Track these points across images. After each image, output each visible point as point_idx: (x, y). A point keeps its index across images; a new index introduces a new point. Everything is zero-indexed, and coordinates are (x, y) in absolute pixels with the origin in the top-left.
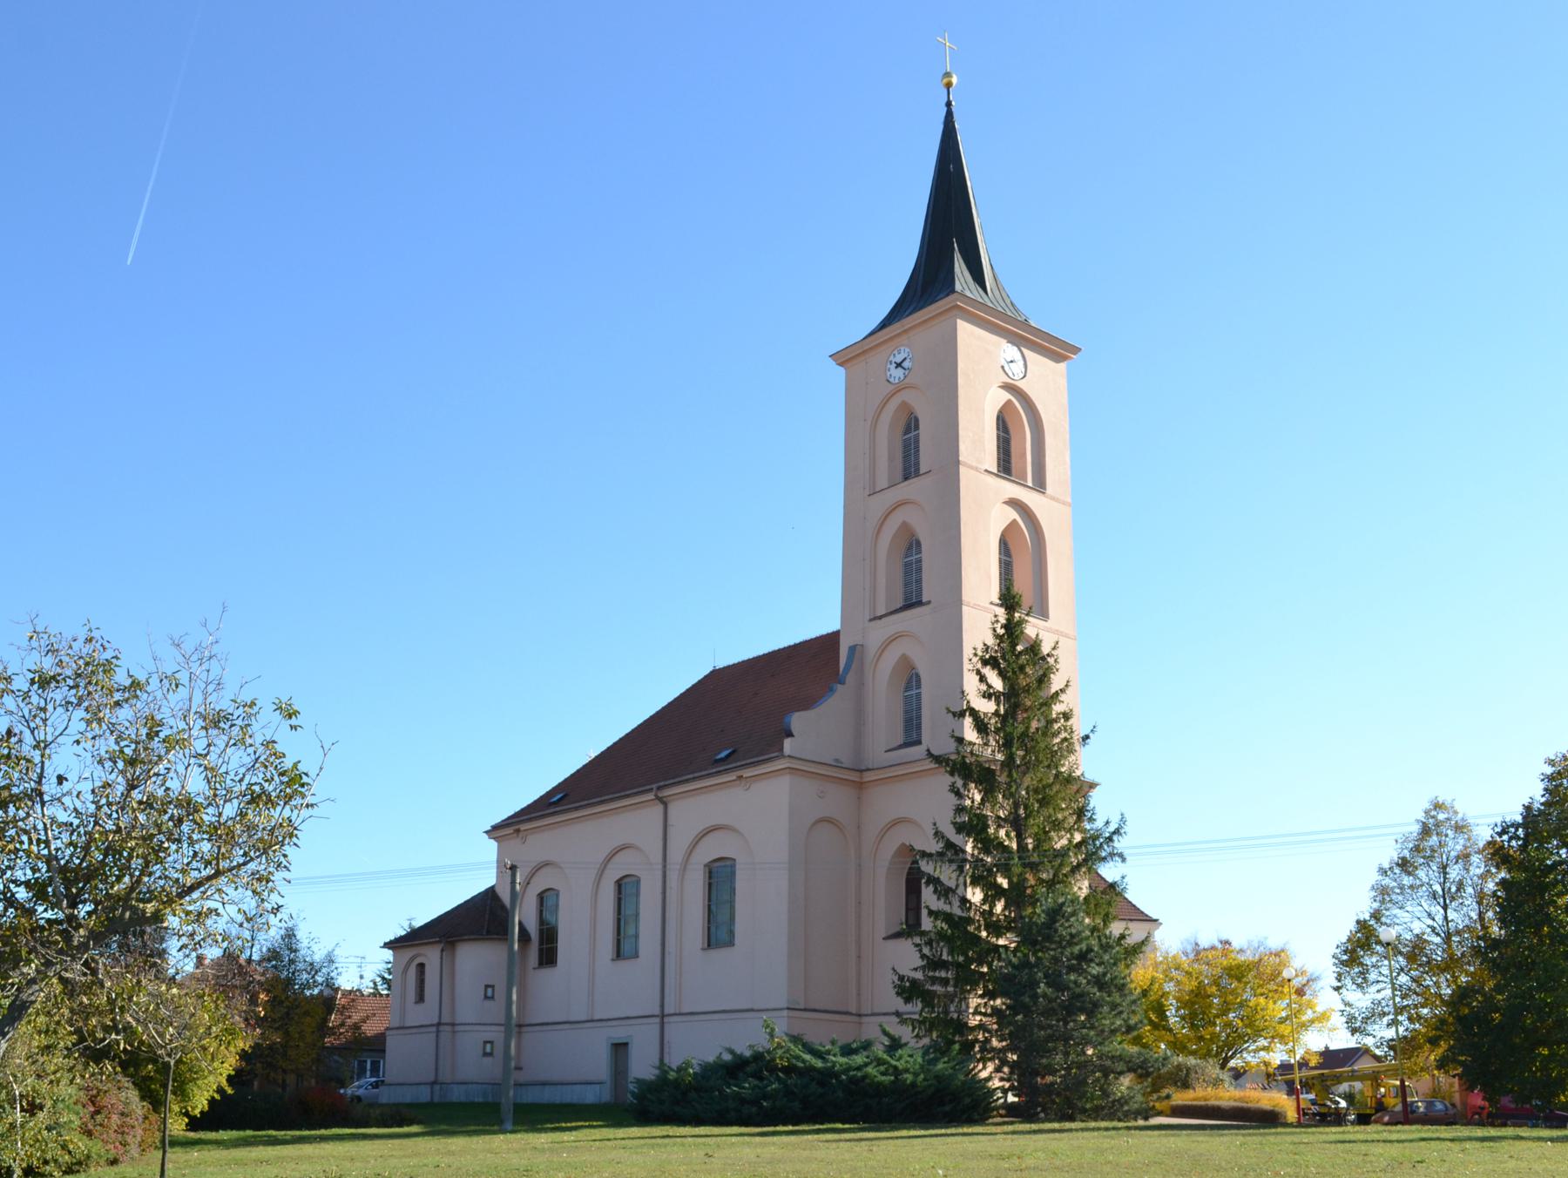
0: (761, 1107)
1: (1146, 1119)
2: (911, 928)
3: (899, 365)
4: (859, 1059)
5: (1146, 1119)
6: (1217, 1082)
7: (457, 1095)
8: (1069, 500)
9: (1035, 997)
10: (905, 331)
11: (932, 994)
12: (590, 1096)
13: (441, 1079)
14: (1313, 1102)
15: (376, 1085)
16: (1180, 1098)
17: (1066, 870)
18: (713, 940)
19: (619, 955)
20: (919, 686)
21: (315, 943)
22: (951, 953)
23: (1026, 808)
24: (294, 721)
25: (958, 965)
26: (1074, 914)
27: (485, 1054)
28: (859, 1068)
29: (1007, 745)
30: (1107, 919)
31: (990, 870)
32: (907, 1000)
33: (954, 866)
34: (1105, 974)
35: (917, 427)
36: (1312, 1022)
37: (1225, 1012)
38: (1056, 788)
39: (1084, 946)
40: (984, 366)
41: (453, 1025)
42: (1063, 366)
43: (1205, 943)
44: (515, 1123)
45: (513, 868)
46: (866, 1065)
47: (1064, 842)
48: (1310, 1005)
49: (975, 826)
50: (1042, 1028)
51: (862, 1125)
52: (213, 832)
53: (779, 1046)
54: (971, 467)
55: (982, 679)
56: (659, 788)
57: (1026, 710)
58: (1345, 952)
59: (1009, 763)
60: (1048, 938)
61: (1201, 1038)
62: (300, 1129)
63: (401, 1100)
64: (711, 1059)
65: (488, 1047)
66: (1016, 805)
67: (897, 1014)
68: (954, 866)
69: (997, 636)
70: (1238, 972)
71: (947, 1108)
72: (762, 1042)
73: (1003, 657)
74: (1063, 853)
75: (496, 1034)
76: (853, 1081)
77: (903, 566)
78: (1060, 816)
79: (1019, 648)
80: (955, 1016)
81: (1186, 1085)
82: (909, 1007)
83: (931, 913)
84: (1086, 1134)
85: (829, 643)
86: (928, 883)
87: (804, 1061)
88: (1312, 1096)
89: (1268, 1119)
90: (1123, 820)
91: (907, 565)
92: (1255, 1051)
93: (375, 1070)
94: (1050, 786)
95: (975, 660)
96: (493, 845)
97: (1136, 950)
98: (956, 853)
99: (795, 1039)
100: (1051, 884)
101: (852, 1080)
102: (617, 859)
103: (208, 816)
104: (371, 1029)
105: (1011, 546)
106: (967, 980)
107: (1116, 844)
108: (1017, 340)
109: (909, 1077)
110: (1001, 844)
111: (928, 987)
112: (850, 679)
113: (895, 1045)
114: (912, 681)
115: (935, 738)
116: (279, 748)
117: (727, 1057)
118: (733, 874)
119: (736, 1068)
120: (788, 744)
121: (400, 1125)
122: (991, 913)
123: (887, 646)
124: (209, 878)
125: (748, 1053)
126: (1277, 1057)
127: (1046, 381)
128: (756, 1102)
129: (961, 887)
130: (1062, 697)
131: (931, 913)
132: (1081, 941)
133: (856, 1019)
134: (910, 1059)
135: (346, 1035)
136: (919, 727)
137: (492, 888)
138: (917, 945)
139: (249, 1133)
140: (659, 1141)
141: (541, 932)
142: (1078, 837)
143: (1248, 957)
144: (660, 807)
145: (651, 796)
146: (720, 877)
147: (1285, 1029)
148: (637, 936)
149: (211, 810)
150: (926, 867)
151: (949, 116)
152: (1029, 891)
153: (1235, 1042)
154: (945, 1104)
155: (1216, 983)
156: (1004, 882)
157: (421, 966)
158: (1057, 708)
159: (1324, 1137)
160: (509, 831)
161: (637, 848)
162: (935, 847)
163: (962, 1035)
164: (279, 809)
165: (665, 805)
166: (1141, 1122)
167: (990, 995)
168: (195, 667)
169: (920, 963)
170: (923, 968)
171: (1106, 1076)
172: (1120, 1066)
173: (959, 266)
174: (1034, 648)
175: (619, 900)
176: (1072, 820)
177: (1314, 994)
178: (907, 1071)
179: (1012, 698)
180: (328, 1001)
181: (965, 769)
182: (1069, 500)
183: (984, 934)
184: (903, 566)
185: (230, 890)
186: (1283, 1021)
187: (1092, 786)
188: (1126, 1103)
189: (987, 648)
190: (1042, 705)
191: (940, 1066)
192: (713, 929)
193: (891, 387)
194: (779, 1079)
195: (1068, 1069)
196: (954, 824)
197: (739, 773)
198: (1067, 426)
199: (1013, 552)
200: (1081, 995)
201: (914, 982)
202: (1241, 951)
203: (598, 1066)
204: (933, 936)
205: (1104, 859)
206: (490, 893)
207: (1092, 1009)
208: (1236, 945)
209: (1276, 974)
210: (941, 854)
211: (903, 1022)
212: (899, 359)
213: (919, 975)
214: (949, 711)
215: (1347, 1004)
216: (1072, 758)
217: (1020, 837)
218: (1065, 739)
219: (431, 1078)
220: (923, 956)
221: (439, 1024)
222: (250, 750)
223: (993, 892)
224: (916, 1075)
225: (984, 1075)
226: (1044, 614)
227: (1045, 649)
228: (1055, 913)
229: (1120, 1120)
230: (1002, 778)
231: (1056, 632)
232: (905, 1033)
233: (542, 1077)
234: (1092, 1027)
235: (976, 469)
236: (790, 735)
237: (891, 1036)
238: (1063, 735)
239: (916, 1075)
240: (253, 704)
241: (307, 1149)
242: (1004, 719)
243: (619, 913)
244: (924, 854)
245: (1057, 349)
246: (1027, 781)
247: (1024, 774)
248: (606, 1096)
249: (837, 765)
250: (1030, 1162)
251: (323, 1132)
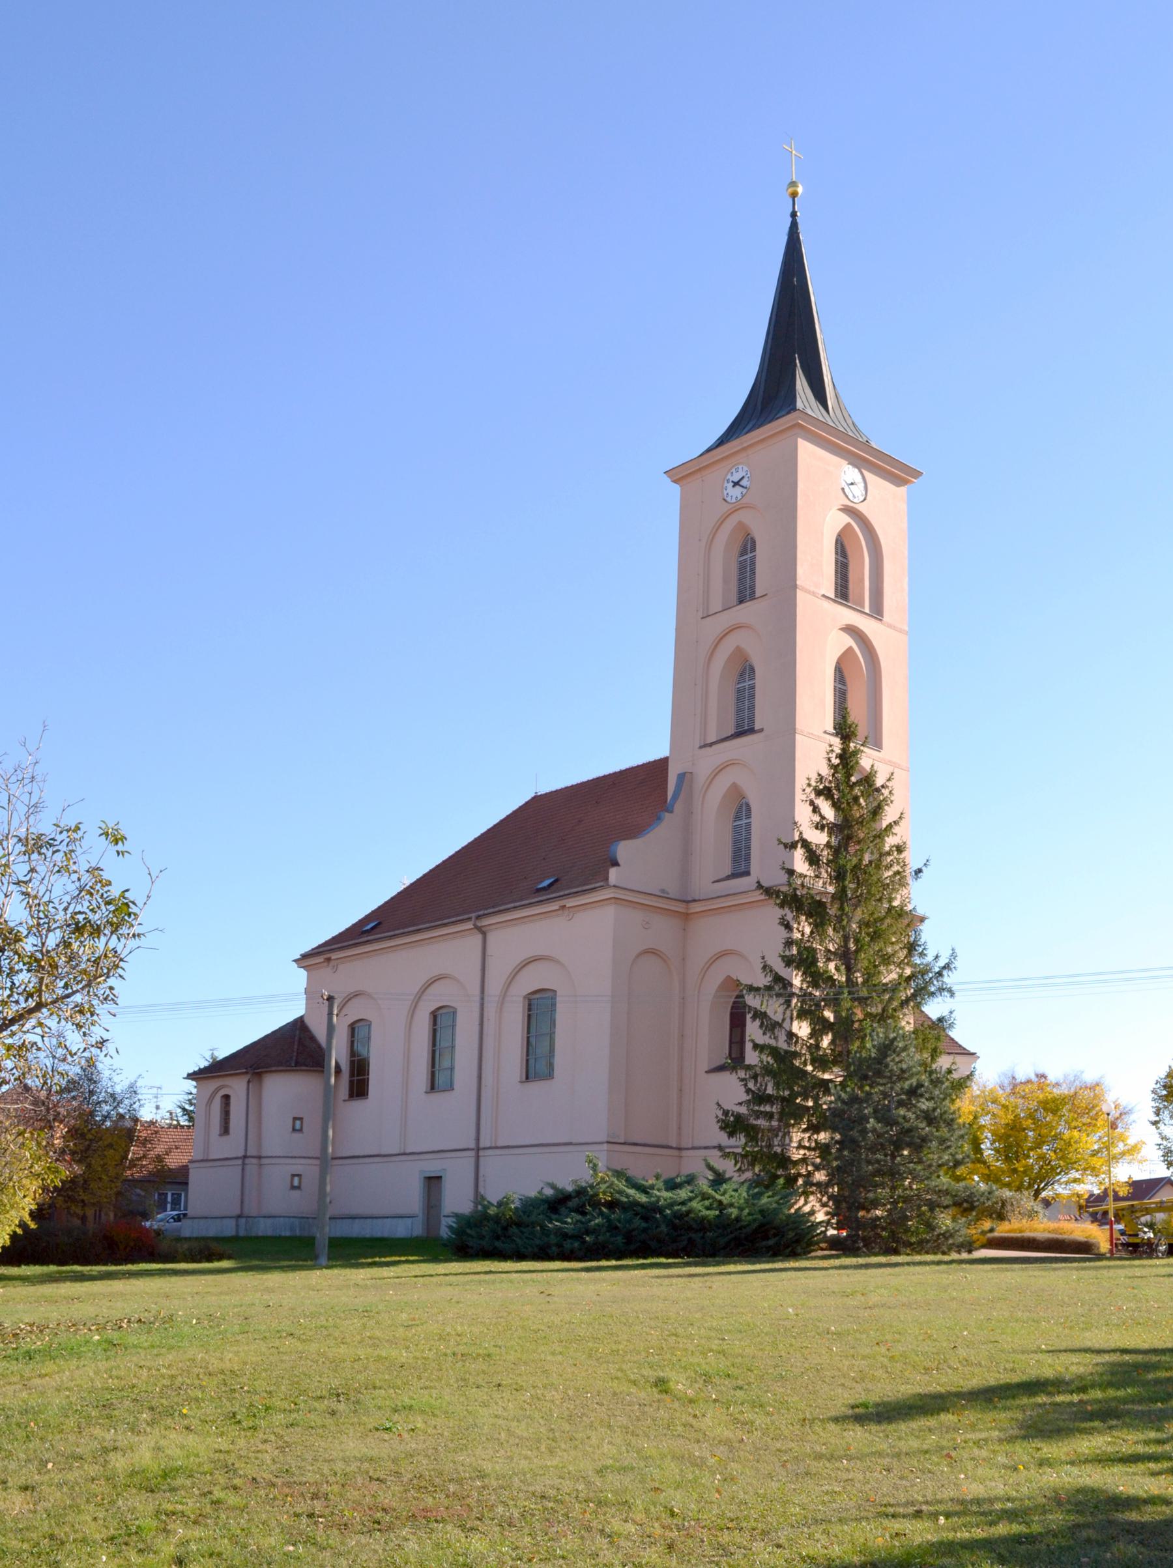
0: (584, 1242)
1: (970, 1252)
2: (735, 1061)
3: (736, 484)
4: (683, 1194)
5: (970, 1252)
6: (1031, 1214)
7: (264, 1228)
8: (906, 628)
9: (864, 1132)
10: (744, 449)
11: (756, 1129)
12: (401, 1230)
13: (246, 1212)
14: (1123, 1233)
15: (178, 1219)
16: (1003, 1230)
17: (895, 1004)
18: (532, 1072)
19: (433, 1087)
20: (749, 815)
21: (116, 1073)
22: (777, 1086)
23: (857, 941)
24: (120, 847)
25: (783, 1099)
26: (905, 1049)
27: (293, 1188)
28: (683, 1203)
29: (839, 876)
30: (935, 1053)
31: (818, 1005)
32: (731, 1134)
33: (782, 1000)
34: (934, 1109)
35: (753, 549)
36: (1123, 1154)
37: (1038, 1145)
38: (888, 921)
39: (914, 1081)
40: (826, 487)
41: (260, 1157)
42: (903, 490)
43: (1021, 1077)
44: (329, 1259)
45: (330, 999)
46: (691, 1199)
47: (894, 976)
48: (1122, 1138)
49: (805, 961)
50: (869, 1162)
51: (686, 1259)
52: (34, 963)
53: (603, 1181)
54: (809, 592)
55: (816, 809)
56: (478, 917)
57: (859, 842)
58: (1165, 1087)
59: (840, 896)
60: (879, 1073)
61: (1015, 1171)
62: (105, 1264)
63: (204, 1234)
64: (533, 1194)
65: (296, 1180)
66: (846, 939)
67: (720, 1148)
68: (782, 1000)
69: (832, 766)
70: (1053, 1106)
71: (771, 1242)
72: (584, 1176)
73: (837, 788)
74: (894, 988)
75: (310, 1171)
76: (679, 1216)
77: (737, 695)
78: (889, 950)
79: (853, 779)
80: (779, 1150)
81: (1001, 1217)
82: (732, 1141)
83: (756, 1046)
84: (912, 1269)
85: (659, 768)
86: (754, 1018)
87: (627, 1196)
88: (1121, 1227)
89: (1084, 1249)
90: (953, 955)
91: (740, 691)
92: (1067, 1183)
93: (176, 1203)
94: (882, 920)
95: (808, 790)
96: (303, 973)
97: (961, 1085)
98: (785, 987)
99: (619, 1174)
100: (882, 1018)
101: (677, 1215)
102: (431, 990)
103: (29, 945)
104: (174, 1161)
105: (846, 674)
106: (791, 1113)
107: (946, 979)
108: (858, 462)
109: (734, 1212)
110: (831, 978)
111: (753, 1121)
112: (678, 807)
113: (719, 1180)
114: (743, 811)
115: (764, 869)
116: (106, 875)
117: (549, 1192)
118: (554, 1005)
119: (558, 1203)
120: (613, 873)
121: (209, 1260)
122: (817, 1047)
123: (716, 774)
124: (31, 1011)
125: (570, 1188)
126: (1090, 1186)
127: (886, 505)
128: (578, 1237)
129: (788, 1020)
130: (896, 829)
131: (756, 1046)
132: (912, 1076)
133: (675, 1152)
134: (735, 1196)
135: (148, 1166)
136: (748, 858)
137: (301, 1018)
138: (742, 1080)
139: (53, 1268)
140: (483, 1277)
141: (352, 1063)
142: (908, 971)
143: (1064, 1090)
144: (478, 938)
145: (469, 925)
146: (539, 1009)
147: (1096, 1162)
148: (452, 1069)
149: (32, 940)
150: (752, 1001)
151: (794, 227)
152: (856, 1025)
153: (1046, 1175)
154: (767, 1239)
155: (1031, 1116)
156: (829, 1015)
157: (227, 1098)
158: (890, 841)
159: (1154, 1271)
160: (320, 959)
161: (455, 979)
162: (762, 980)
163: (785, 1168)
164: (103, 939)
165: (484, 934)
166: (965, 1256)
167: (814, 1129)
168: (15, 789)
169: (746, 1097)
170: (748, 1102)
171: (932, 1210)
172: (947, 1201)
173: (801, 384)
174: (868, 780)
175: (435, 1031)
176: (902, 954)
177: (1127, 1128)
178: (731, 1205)
179: (844, 831)
180: (127, 1131)
181: (796, 901)
182: (906, 628)
183: (809, 1068)
184: (737, 695)
185: (52, 1023)
186: (1095, 1153)
187: (922, 920)
188: (951, 1236)
189: (821, 778)
190: (875, 837)
191: (764, 1200)
192: (532, 1062)
193: (726, 508)
194: (601, 1214)
195: (895, 1203)
196: (783, 957)
197: (562, 903)
198: (906, 553)
200: (909, 1130)
201: (738, 1117)
202: (1057, 1084)
203: (412, 1199)
204: (758, 1070)
205: (933, 994)
206: (299, 1025)
207: (919, 1146)
208: (1052, 1078)
209: (1089, 1109)
210: (769, 988)
211: (726, 1155)
212: (736, 478)
213: (743, 1110)
214: (780, 842)
215: (1164, 1138)
216: (904, 892)
217: (849, 970)
218: (898, 873)
219: (237, 1212)
220: (748, 1091)
221: (245, 1157)
222: (74, 877)
223: (820, 1027)
224: (741, 1209)
225: (807, 1209)
226: (878, 745)
227: (879, 782)
228: (887, 1048)
229: (944, 1253)
230: (833, 911)
231: (889, 763)
232: (727, 1167)
233: (355, 1211)
234: (920, 1162)
235: (814, 594)
236: (615, 864)
237: (704, 1166)
238: (896, 868)
239: (741, 1209)
240: (77, 829)
241: (117, 1285)
242: (837, 851)
243: (434, 1044)
244: (751, 989)
245: (898, 473)
246: (859, 914)
247: (856, 906)
248: (418, 1230)
249: (663, 895)
250: (874, 1299)
251: (130, 1267)
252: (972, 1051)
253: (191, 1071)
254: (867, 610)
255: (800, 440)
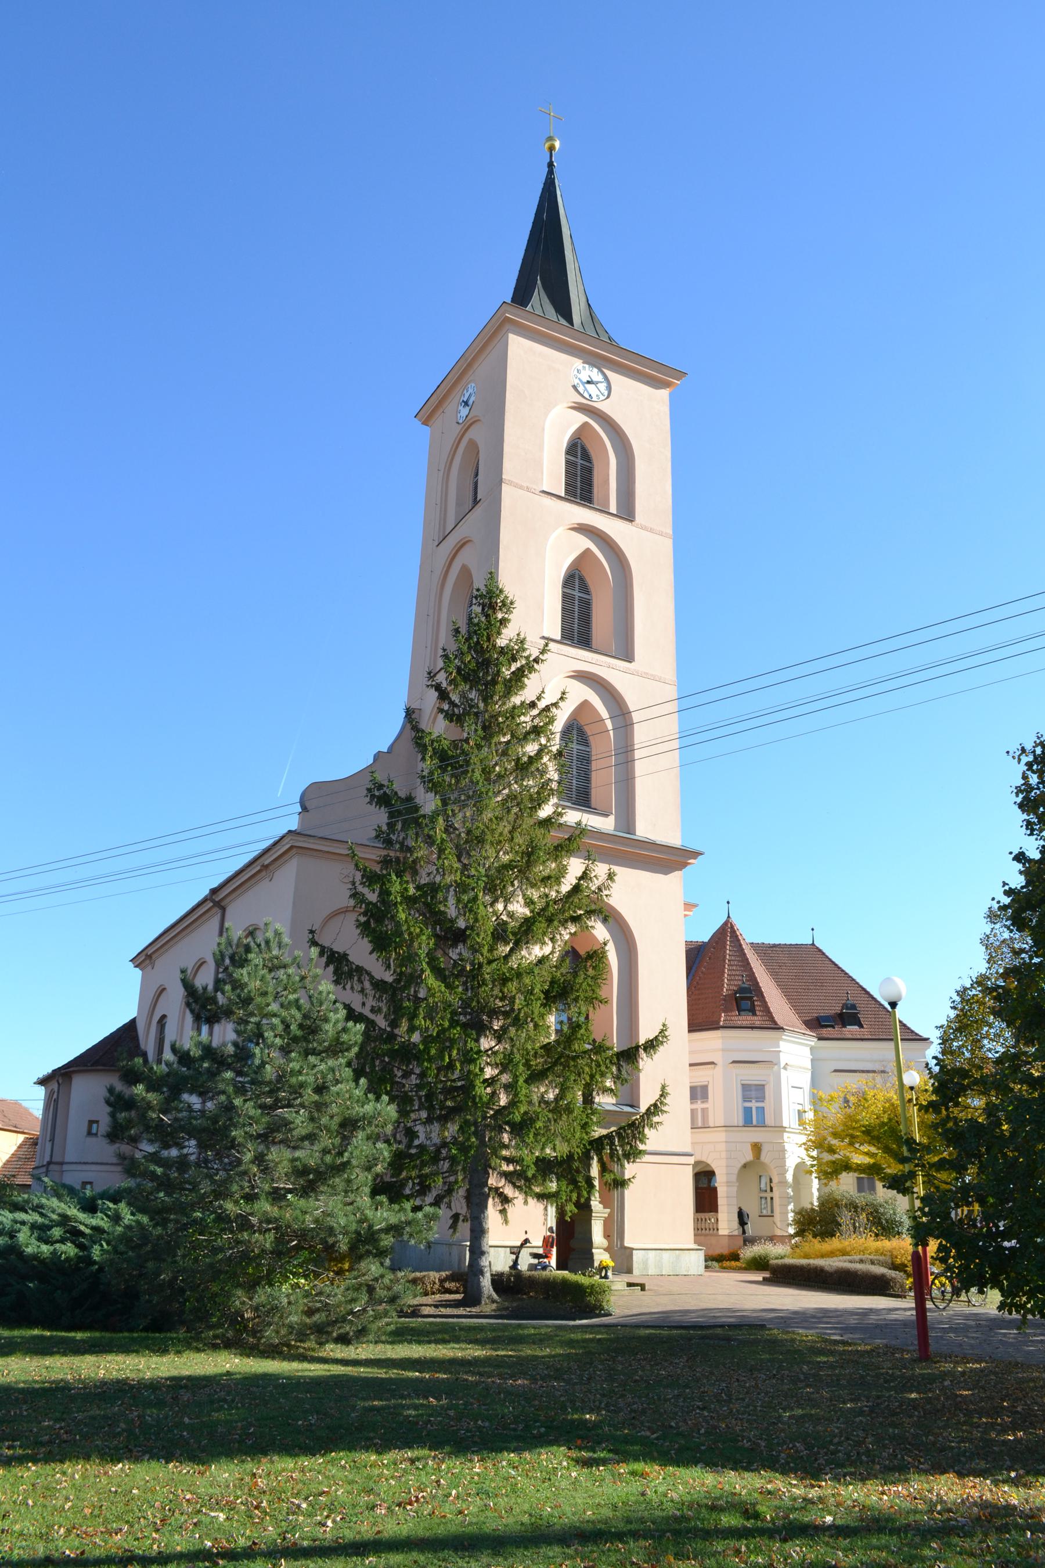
41: (62, 1164)
127: (641, 411)
165: (223, 909)
199: (592, 588)
221: (49, 1163)
245: (652, 372)
252: (925, 1036)
253: (41, 1076)
254: (613, 509)
255: (511, 336)
